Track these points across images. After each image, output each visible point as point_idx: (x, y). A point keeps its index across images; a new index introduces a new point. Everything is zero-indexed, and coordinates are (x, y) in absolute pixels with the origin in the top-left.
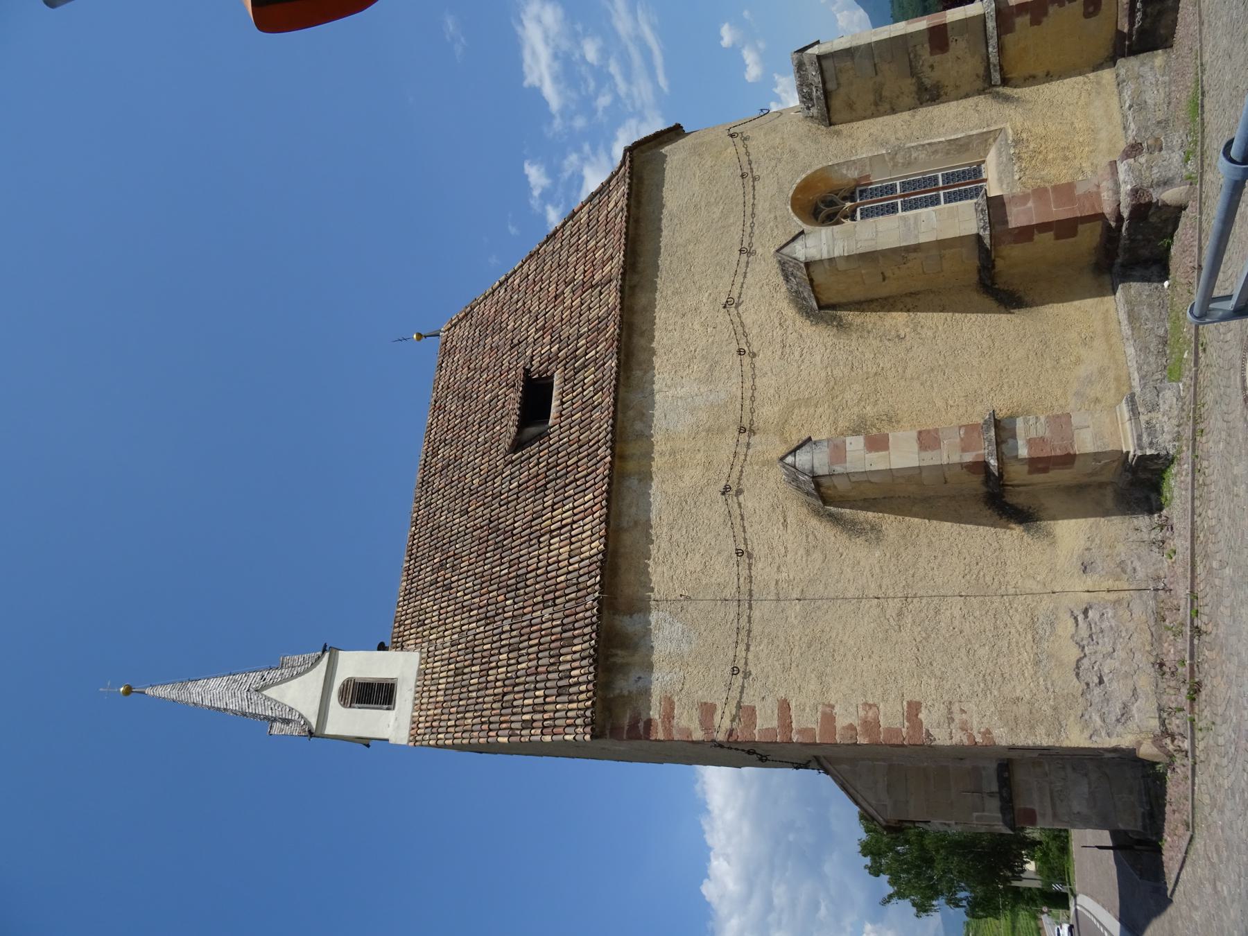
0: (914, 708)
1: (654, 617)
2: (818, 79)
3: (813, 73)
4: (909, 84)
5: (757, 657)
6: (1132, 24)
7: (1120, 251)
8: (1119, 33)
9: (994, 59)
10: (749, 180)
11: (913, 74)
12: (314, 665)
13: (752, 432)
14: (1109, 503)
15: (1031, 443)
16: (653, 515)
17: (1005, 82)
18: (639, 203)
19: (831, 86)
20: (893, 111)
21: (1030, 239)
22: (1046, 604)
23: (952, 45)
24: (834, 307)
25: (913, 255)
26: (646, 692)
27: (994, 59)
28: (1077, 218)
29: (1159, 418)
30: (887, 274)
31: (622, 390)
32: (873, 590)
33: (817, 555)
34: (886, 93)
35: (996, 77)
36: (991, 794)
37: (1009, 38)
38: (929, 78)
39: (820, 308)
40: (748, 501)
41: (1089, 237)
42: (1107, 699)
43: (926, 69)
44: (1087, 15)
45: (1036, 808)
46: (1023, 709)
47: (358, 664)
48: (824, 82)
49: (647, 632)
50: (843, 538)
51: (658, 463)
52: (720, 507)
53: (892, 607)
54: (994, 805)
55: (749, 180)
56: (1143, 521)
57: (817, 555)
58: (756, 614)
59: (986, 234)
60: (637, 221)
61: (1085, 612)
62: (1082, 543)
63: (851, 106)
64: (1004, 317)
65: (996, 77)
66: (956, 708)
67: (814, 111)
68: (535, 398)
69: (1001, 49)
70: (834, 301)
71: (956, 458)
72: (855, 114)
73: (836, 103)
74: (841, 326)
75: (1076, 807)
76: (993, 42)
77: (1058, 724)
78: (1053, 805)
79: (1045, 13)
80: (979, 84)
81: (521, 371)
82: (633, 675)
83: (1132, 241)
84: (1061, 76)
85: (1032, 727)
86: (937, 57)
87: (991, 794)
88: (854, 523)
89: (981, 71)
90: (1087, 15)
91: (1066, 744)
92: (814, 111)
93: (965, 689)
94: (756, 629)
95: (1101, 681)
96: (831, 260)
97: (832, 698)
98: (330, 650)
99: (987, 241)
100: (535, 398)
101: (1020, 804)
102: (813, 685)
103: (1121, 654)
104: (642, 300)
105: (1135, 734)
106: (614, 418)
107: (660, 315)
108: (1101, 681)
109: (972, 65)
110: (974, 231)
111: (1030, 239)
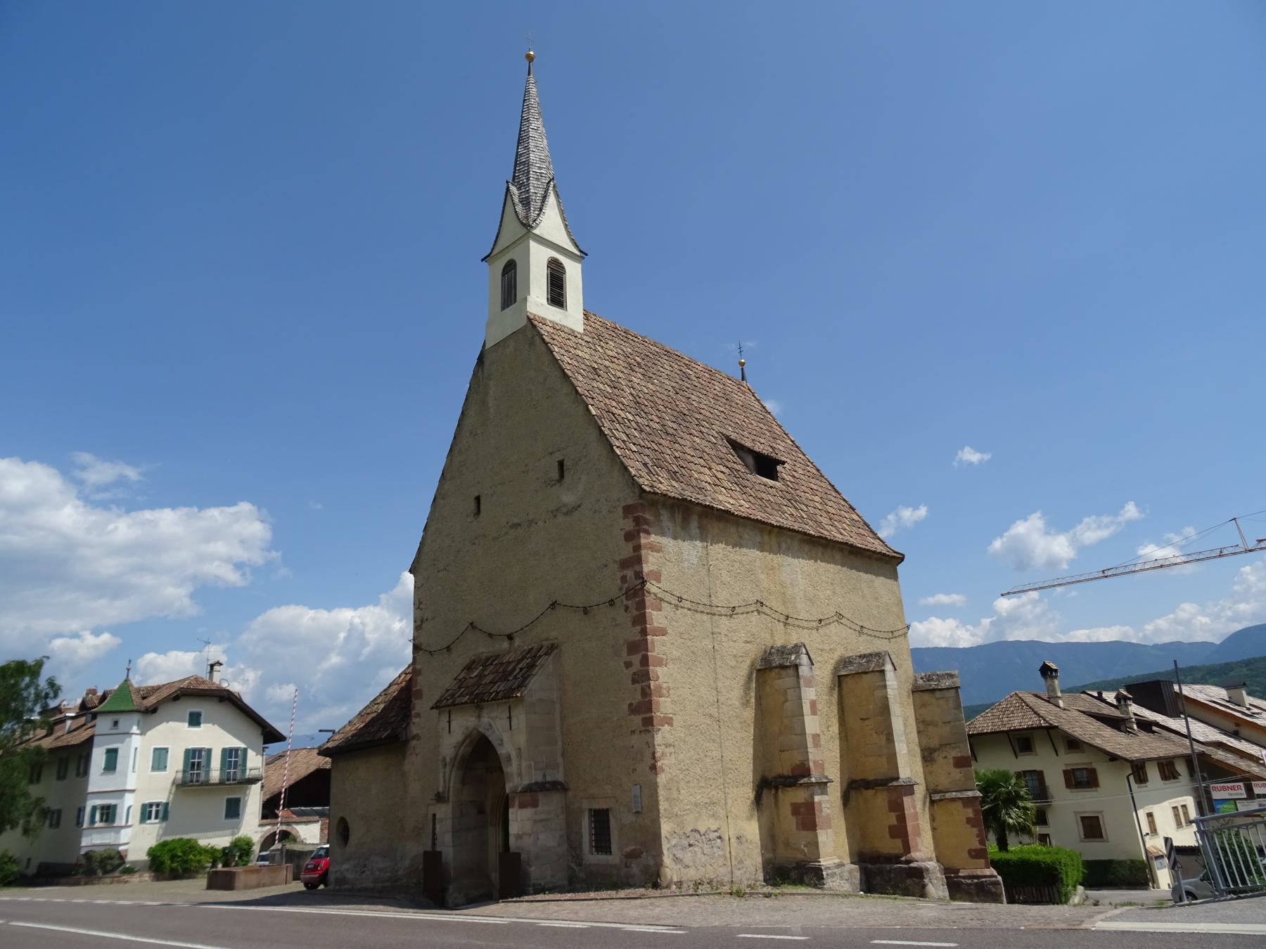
0: (669, 721)
1: (698, 543)
2: (943, 686)
3: (946, 683)
4: (935, 743)
5: (685, 615)
6: (964, 877)
7: (878, 866)
8: (958, 871)
9: (948, 795)
10: (815, 624)
11: (941, 745)
12: (572, 240)
13: (785, 624)
14: (769, 855)
15: (820, 803)
16: (745, 550)
17: (932, 802)
18: (877, 560)
19: (938, 694)
20: (919, 732)
21: (891, 810)
22: (722, 813)
23: (958, 770)
24: (840, 686)
25: (883, 738)
26: (663, 534)
27: (948, 795)
28: (907, 836)
29: (837, 879)
30: (867, 722)
31: (800, 536)
32: (722, 699)
33: (733, 663)
34: (930, 728)
35: (937, 797)
36: (545, 776)
37: (959, 805)
38: (938, 756)
39: (839, 677)
40: (754, 617)
41: (890, 846)
42: (683, 849)
43: (944, 754)
44: (970, 851)
45: (539, 809)
46: (675, 794)
47: (573, 273)
48: (941, 690)
49: (692, 538)
50: (742, 682)
51: (770, 556)
52: (752, 599)
53: (713, 711)
54: (537, 777)
55: (815, 624)
56: (761, 876)
57: (733, 663)
58: (705, 617)
59: (901, 782)
60: (870, 557)
61: (720, 837)
62: (750, 837)
63: (924, 705)
64: (839, 794)
65: (937, 797)
66: (672, 750)
67: (921, 682)
68: (766, 466)
69: (953, 800)
70: (844, 685)
71: (811, 757)
72: (918, 707)
73: (926, 696)
74: (832, 689)
75: (542, 837)
76: (959, 795)
77: (672, 816)
78: (541, 821)
79: (973, 826)
80: (932, 786)
81: (783, 459)
82: (670, 525)
83: (890, 872)
84: (934, 837)
85: (668, 799)
86: (951, 761)
87: (545, 776)
88: (749, 689)
89: (940, 788)
90: (970, 851)
91: (662, 821)
92: (921, 682)
93: (681, 756)
94: (698, 616)
95: (690, 845)
96: (885, 687)
97: (670, 666)
98: (582, 256)
99: (895, 783)
100: (766, 466)
101: (541, 796)
102: (676, 653)
103: (704, 859)
104: (838, 556)
105: (671, 870)
106: (789, 529)
107: (822, 566)
108: (690, 845)
109: (944, 782)
110: (902, 776)
111: (891, 810)
